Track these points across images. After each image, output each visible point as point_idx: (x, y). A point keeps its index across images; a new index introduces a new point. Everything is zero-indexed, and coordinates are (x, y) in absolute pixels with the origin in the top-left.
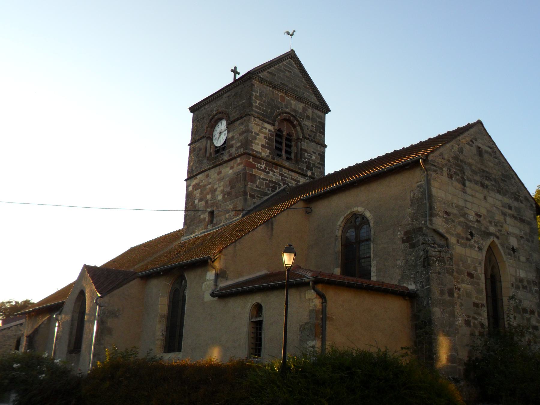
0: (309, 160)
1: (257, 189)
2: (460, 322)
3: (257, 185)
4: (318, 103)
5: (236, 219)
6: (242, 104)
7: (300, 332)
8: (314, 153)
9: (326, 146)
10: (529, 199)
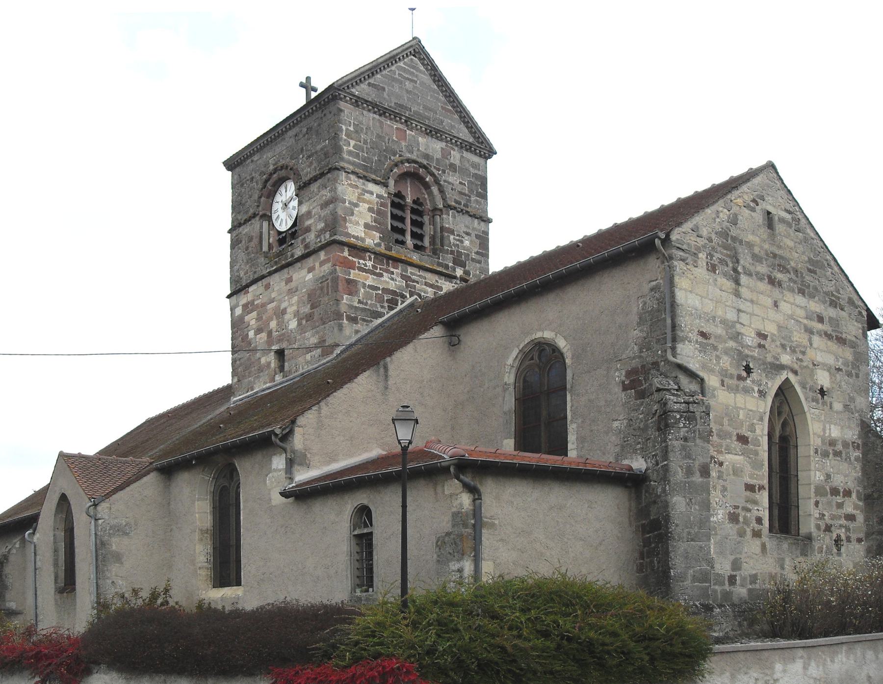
0: (458, 248)
1: (361, 306)
2: (719, 517)
3: (361, 298)
4: (471, 140)
5: (325, 361)
6: (322, 149)
7: (437, 550)
8: (468, 234)
9: (489, 221)
10: (856, 302)
